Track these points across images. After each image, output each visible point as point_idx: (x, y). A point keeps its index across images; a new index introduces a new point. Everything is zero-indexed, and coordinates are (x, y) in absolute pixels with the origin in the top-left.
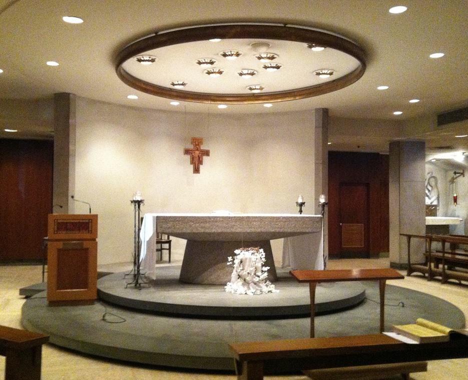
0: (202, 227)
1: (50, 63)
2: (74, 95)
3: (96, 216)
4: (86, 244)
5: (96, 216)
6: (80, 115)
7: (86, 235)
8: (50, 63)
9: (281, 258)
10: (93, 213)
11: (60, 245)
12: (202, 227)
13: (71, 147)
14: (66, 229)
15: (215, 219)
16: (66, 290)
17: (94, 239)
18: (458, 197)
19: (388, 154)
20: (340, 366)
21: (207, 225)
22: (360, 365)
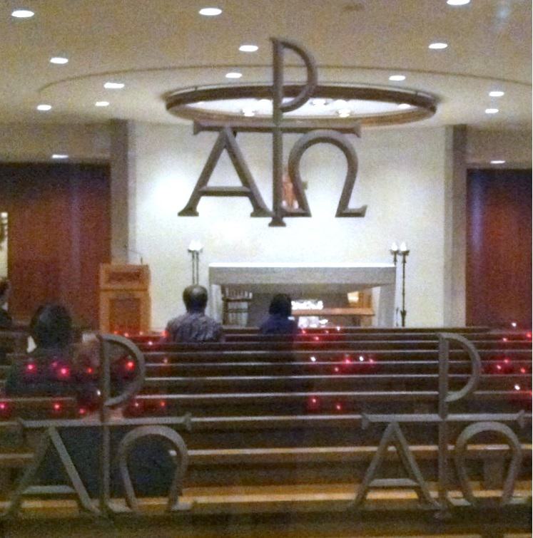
0: (259, 279)
1: (441, 46)
2: (133, 121)
3: (147, 266)
4: (139, 295)
5: (147, 266)
6: (140, 147)
7: (135, 285)
8: (441, 46)
9: (152, 298)
10: (144, 263)
11: (112, 295)
12: (259, 279)
13: (131, 184)
14: (120, 280)
15: (273, 271)
16: (276, 378)
17: (146, 290)
18: (368, 209)
19: (107, 155)
20: (223, 447)
21: (264, 276)
22: (233, 448)
